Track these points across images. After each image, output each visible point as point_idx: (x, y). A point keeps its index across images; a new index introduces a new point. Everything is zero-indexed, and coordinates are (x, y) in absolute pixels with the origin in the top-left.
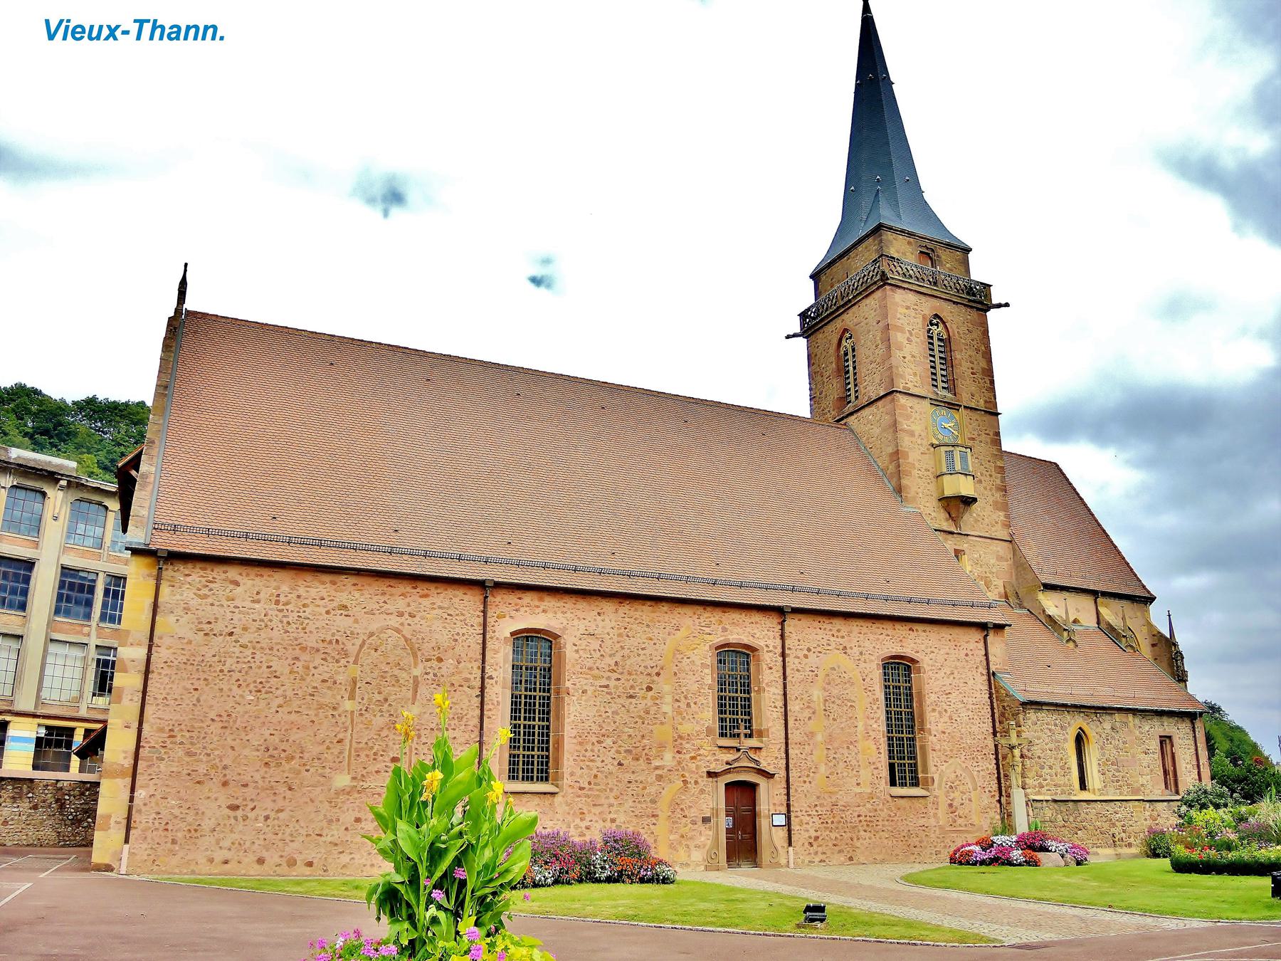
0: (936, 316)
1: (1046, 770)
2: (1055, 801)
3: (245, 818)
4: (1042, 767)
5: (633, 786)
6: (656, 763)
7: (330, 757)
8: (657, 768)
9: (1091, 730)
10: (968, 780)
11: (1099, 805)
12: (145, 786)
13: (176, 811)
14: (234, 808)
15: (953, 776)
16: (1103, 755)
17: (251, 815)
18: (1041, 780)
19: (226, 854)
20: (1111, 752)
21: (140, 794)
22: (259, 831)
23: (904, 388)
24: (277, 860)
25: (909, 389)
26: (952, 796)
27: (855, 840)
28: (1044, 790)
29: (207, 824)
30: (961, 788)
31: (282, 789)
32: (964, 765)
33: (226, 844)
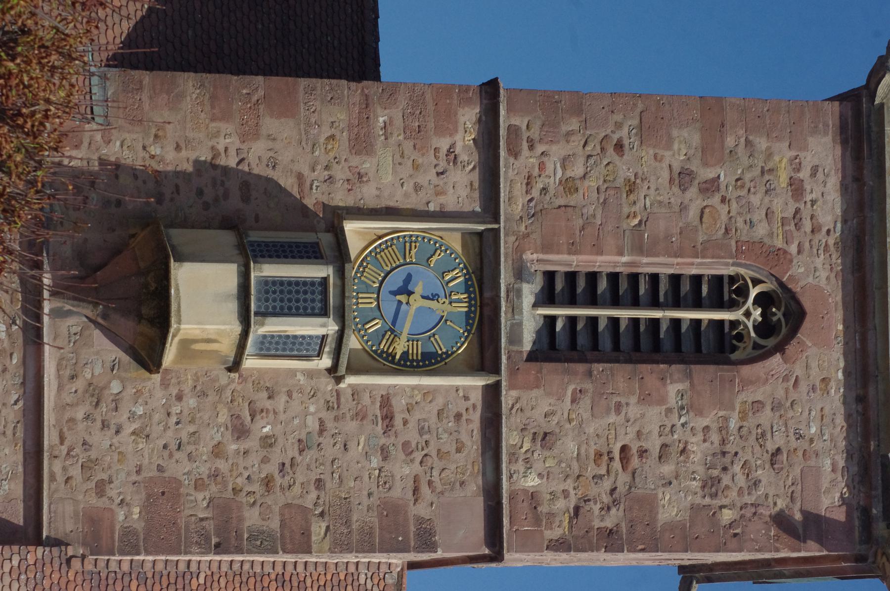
23: (513, 131)
25: (514, 153)
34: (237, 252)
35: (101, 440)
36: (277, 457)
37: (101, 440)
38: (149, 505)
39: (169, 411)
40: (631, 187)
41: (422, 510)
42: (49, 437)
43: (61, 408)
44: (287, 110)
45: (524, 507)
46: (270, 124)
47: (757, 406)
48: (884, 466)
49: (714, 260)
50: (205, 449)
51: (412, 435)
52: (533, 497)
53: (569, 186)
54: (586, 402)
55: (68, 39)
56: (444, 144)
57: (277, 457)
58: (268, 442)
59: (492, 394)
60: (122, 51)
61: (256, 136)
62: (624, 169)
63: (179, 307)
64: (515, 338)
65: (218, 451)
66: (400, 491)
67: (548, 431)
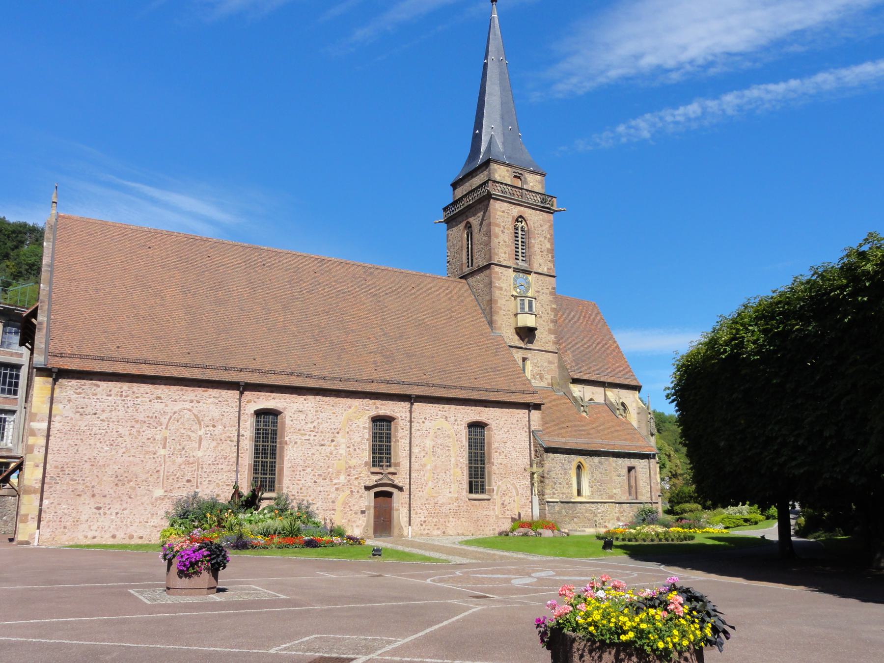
0: (521, 217)
1: (558, 485)
2: (562, 502)
3: (105, 514)
5: (322, 494)
6: (335, 481)
8: (336, 484)
10: (514, 490)
13: (66, 511)
14: (99, 508)
15: (505, 488)
16: (593, 477)
18: (554, 490)
21: (46, 502)
23: (498, 261)
25: (501, 262)
26: (504, 499)
28: (555, 496)
29: (84, 517)
30: (509, 494)
31: (125, 498)
32: (512, 482)
36: (544, 311)
37: (543, 340)
38: (551, 334)
40: (505, 242)
41: (550, 288)
42: (543, 349)
46: (499, 305)
47: (534, 227)
48: (352, 659)
51: (541, 288)
52: (548, 269)
53: (505, 253)
54: (535, 257)
55: (682, 516)
57: (544, 311)
59: (535, 273)
60: (380, 657)
62: (502, 243)
63: (381, 381)
64: (527, 268)
65: (544, 321)
66: (548, 291)
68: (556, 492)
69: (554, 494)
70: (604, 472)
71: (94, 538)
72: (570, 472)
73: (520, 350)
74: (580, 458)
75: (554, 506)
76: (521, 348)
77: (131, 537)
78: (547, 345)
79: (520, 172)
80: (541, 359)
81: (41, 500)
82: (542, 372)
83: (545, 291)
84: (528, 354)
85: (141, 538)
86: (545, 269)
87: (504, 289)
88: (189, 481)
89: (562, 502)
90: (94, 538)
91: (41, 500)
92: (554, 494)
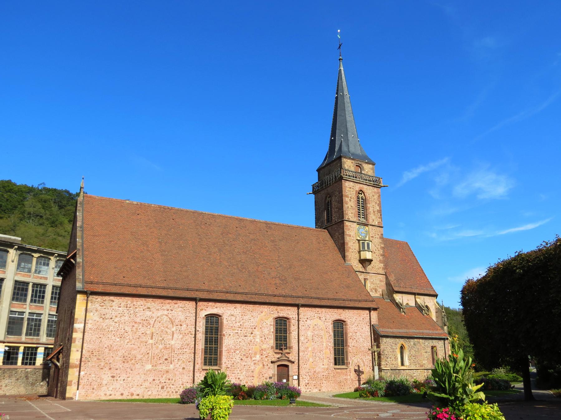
0: (361, 190)
1: (389, 359)
2: (391, 370)
3: (117, 380)
4: (387, 358)
5: (246, 367)
6: (253, 359)
7: (144, 359)
9: (406, 346)
11: (407, 371)
12: (84, 370)
13: (94, 379)
15: (357, 361)
16: (410, 353)
17: (119, 379)
18: (387, 362)
19: (111, 393)
20: (413, 352)
22: (121, 384)
23: (348, 218)
24: (127, 394)
25: (349, 219)
27: (321, 384)
29: (104, 382)
31: (129, 370)
32: (361, 358)
33: (111, 389)
34: (460, 300)
35: (377, 267)
36: (376, 249)
39: (461, 321)
41: (380, 234)
43: (374, 271)
44: (347, 244)
45: (379, 224)
46: (349, 246)
49: (371, 408)
50: (376, 257)
51: (374, 234)
52: (378, 223)
53: (352, 213)
56: (349, 227)
57: (376, 249)
58: (375, 250)
61: (350, 247)
62: (350, 207)
67: (358, 258)
68: (388, 363)
69: (387, 364)
70: (417, 350)
71: (110, 395)
72: (396, 350)
73: (362, 274)
74: (401, 342)
75: (387, 372)
76: (364, 272)
77: (132, 395)
78: (379, 270)
79: (360, 163)
80: (375, 279)
81: (80, 372)
82: (376, 287)
83: (377, 236)
84: (368, 277)
85: (138, 395)
86: (377, 223)
87: (352, 236)
88: (166, 359)
89: (391, 370)
90: (110, 395)
91: (80, 372)
92: (387, 364)
